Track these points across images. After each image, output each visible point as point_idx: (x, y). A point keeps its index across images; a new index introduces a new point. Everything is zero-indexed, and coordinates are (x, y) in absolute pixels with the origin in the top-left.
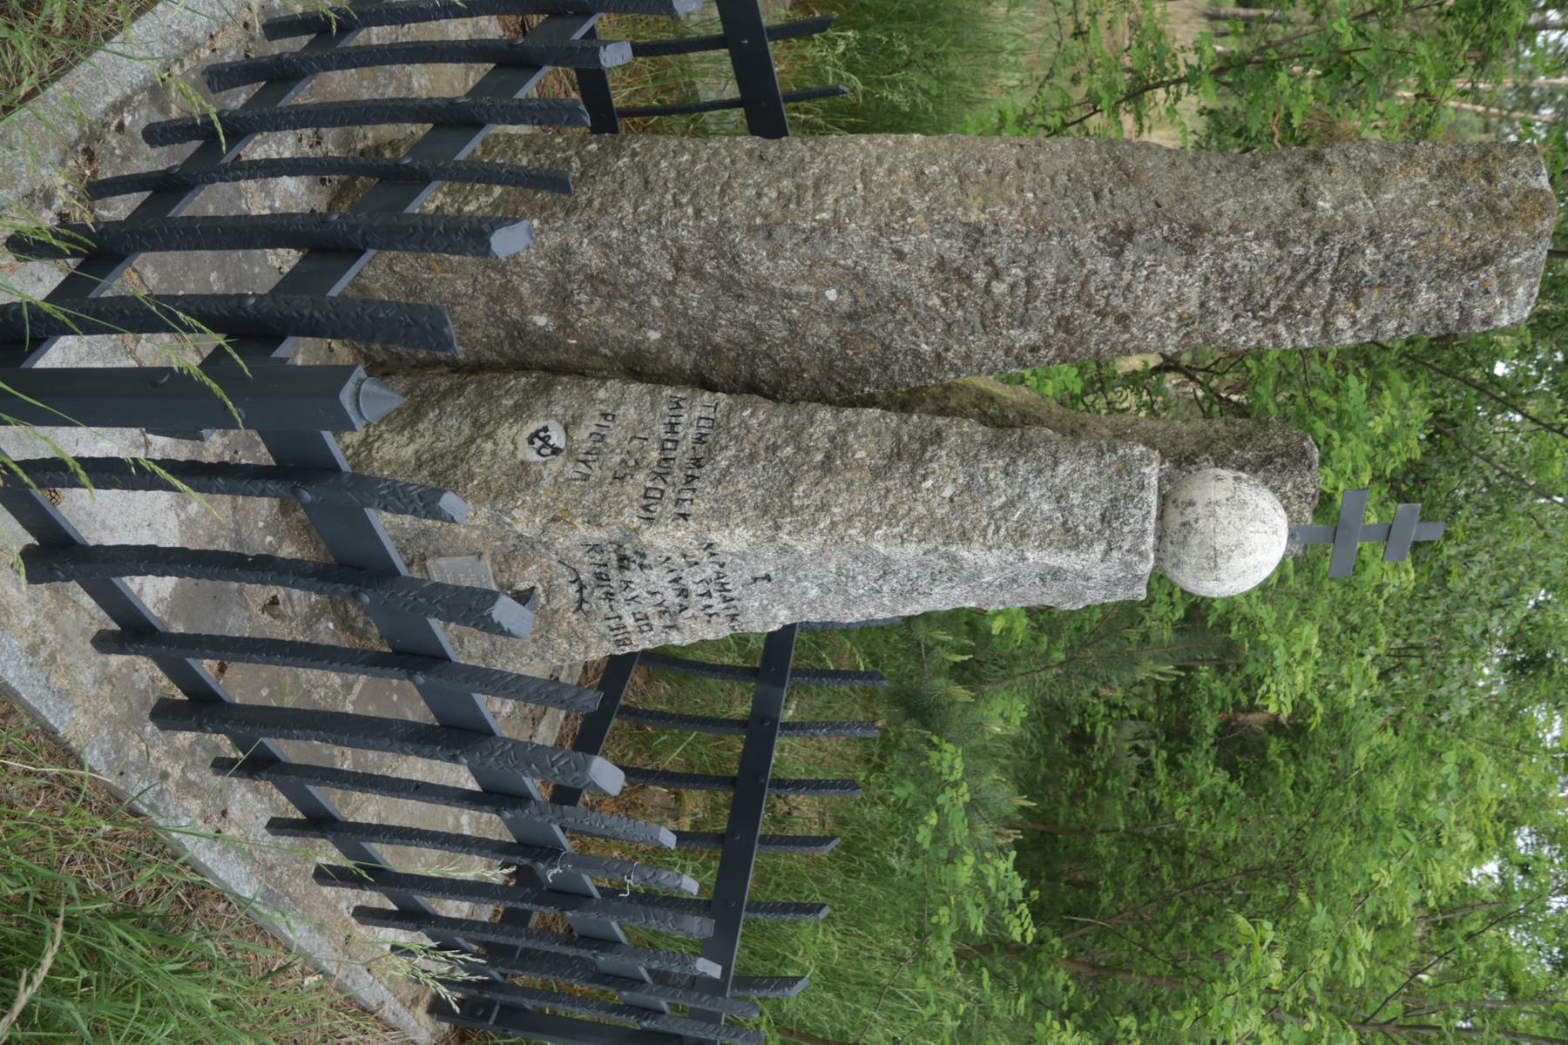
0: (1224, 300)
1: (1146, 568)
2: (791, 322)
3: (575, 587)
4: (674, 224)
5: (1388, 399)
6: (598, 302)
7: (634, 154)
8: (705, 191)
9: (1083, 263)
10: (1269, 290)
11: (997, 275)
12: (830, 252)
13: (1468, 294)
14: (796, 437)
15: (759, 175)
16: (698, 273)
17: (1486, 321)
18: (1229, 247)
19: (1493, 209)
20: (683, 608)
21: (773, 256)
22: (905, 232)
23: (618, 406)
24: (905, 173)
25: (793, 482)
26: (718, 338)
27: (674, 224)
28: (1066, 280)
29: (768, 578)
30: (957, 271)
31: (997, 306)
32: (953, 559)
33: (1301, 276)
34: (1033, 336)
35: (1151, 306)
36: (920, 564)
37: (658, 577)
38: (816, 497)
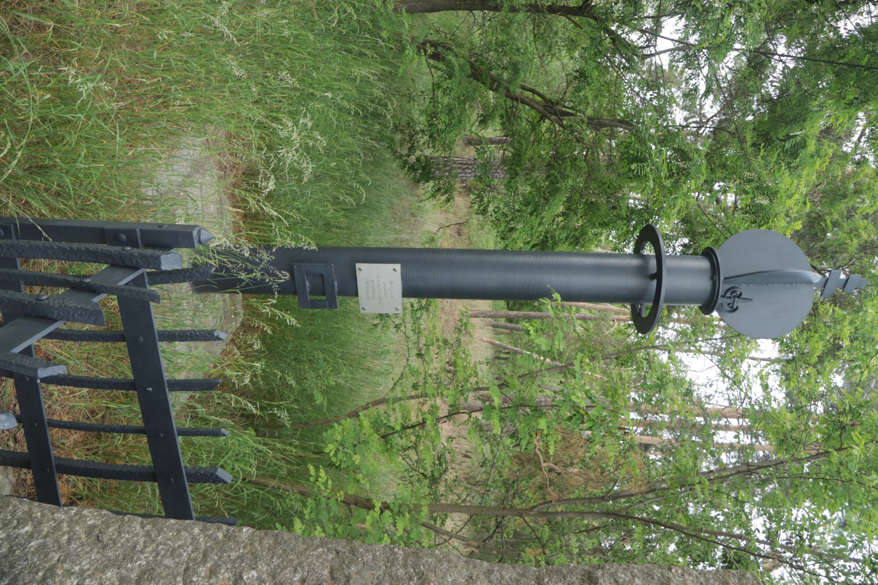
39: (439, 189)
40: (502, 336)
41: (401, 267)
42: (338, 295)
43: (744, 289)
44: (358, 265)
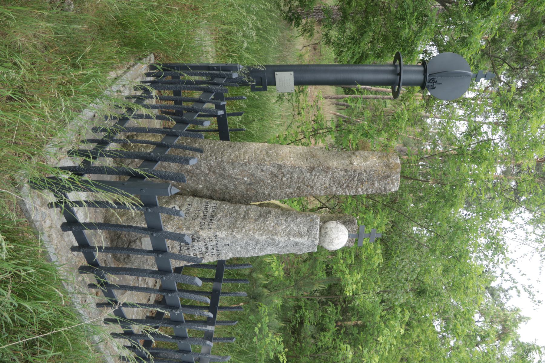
0: (334, 184)
1: (317, 242)
2: (235, 185)
3: (179, 246)
4: (210, 160)
5: (379, 216)
6: (188, 177)
7: (199, 143)
8: (217, 153)
9: (303, 174)
10: (344, 182)
11: (284, 176)
12: (246, 169)
13: (385, 184)
14: (236, 211)
15: (230, 150)
16: (214, 172)
17: (390, 190)
18: (335, 172)
19: (389, 166)
20: (206, 252)
21: (233, 169)
22: (264, 165)
23: (192, 202)
24: (264, 152)
25: (236, 221)
26: (217, 188)
27: (210, 160)
28: (299, 178)
29: (228, 245)
30: (275, 175)
31: (284, 183)
32: (273, 240)
33: (350, 179)
34: (292, 190)
35: (318, 185)
36: (265, 241)
37: (201, 244)
38: (242, 225)
39: (305, 30)
40: (342, 111)
41: (294, 73)
42: (268, 85)
43: (438, 79)
44: (276, 73)
